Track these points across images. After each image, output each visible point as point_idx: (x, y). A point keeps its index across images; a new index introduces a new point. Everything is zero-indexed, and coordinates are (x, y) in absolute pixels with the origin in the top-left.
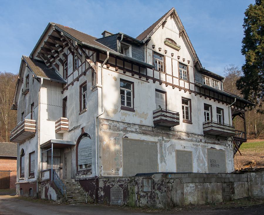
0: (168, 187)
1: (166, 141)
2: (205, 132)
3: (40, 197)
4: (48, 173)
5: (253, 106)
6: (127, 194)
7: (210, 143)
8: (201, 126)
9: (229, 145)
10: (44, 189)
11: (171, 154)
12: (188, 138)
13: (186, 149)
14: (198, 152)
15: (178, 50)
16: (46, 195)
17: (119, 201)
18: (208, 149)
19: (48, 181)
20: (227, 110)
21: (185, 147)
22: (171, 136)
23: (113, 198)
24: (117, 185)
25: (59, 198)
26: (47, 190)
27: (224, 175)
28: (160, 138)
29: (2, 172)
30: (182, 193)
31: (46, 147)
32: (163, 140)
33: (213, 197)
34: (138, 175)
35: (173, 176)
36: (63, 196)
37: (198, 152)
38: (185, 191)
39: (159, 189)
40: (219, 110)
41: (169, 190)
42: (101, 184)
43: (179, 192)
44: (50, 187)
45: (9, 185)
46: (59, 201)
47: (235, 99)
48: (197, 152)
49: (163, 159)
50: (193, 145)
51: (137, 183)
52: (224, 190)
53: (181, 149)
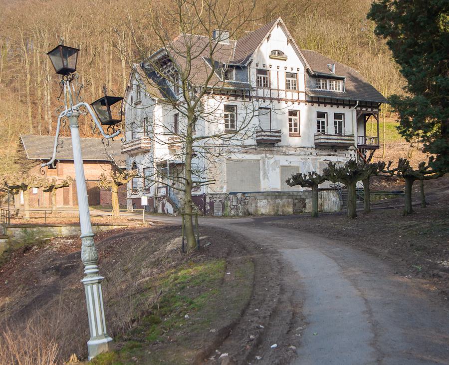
0: (245, 202)
1: (269, 158)
2: (316, 144)
3: (157, 212)
4: (165, 189)
5: (433, 86)
6: (224, 207)
7: (323, 155)
8: (313, 138)
9: (351, 155)
10: (161, 205)
11: (275, 170)
12: (295, 153)
13: (292, 165)
14: (307, 167)
15: (286, 60)
16: (163, 210)
17: (220, 213)
18: (320, 162)
19: (164, 197)
20: (350, 115)
21: (290, 162)
22: (275, 152)
23: (215, 211)
24: (218, 201)
25: (175, 212)
26: (163, 205)
27: (295, 194)
28: (263, 155)
29: (91, 181)
30: (256, 207)
31: (162, 165)
32: (266, 157)
33: (283, 210)
34: (230, 193)
35: (249, 195)
36: (179, 210)
37: (307, 167)
38: (259, 205)
39: (240, 203)
40: (338, 116)
41: (245, 204)
42: (208, 200)
43: (253, 205)
44: (166, 202)
45: (100, 200)
46: (175, 214)
47: (358, 102)
48: (305, 166)
49: (266, 175)
50: (301, 159)
51: (229, 200)
52: (294, 205)
53: (287, 164)
